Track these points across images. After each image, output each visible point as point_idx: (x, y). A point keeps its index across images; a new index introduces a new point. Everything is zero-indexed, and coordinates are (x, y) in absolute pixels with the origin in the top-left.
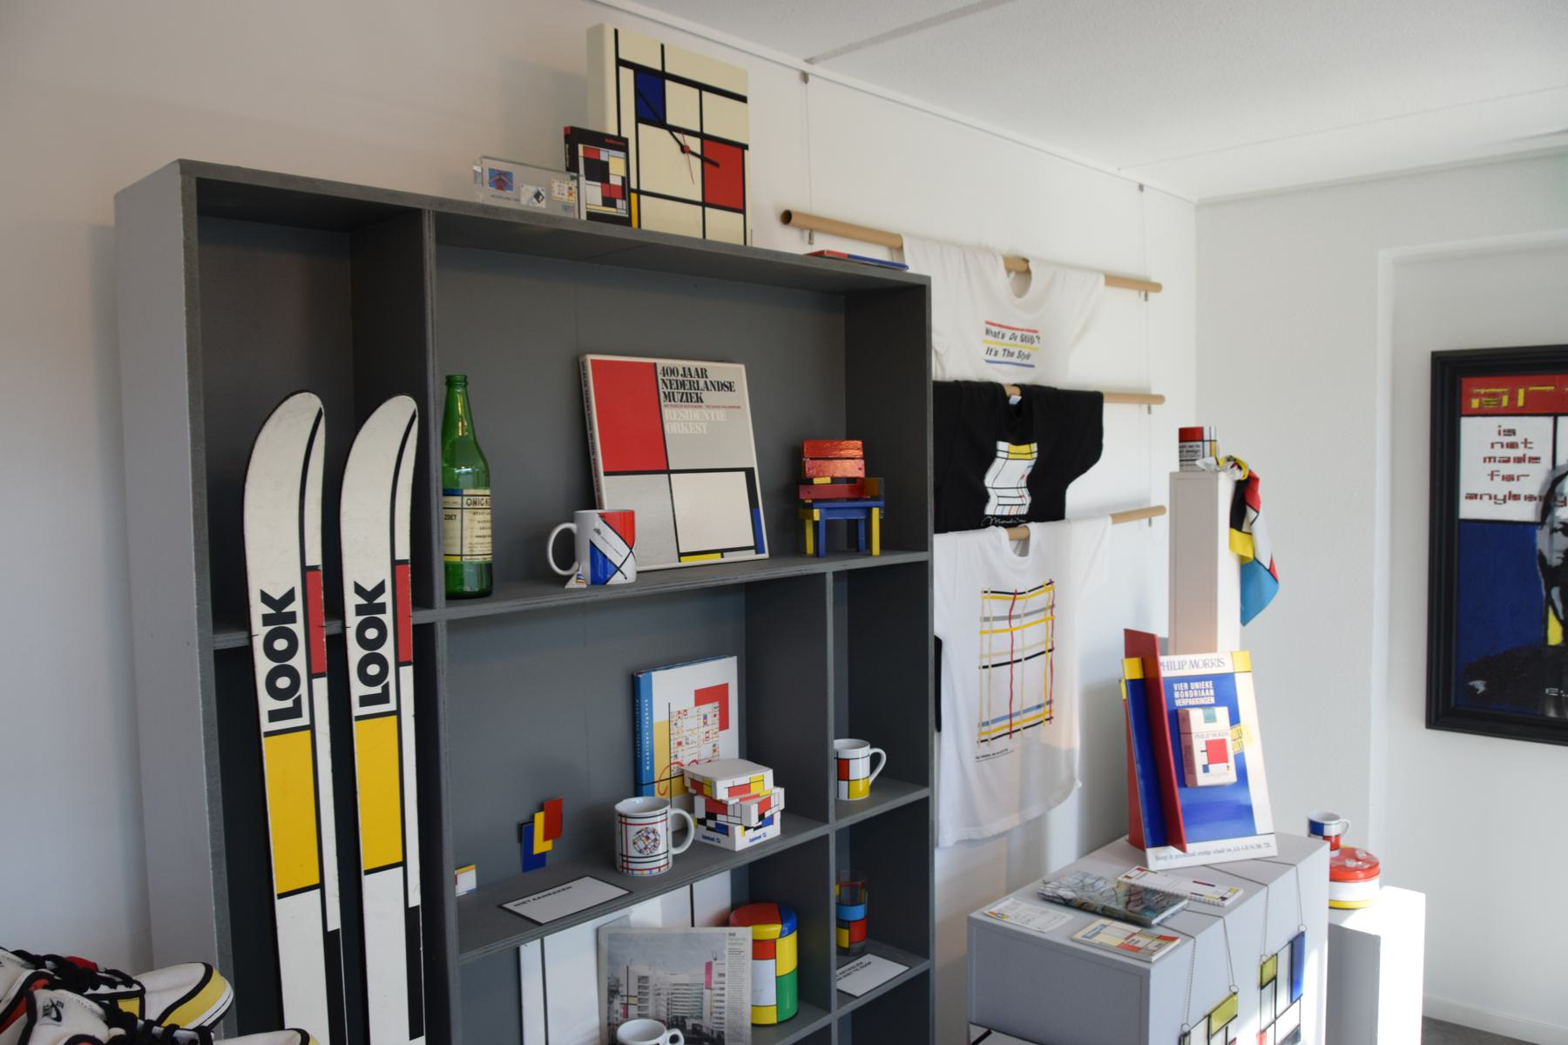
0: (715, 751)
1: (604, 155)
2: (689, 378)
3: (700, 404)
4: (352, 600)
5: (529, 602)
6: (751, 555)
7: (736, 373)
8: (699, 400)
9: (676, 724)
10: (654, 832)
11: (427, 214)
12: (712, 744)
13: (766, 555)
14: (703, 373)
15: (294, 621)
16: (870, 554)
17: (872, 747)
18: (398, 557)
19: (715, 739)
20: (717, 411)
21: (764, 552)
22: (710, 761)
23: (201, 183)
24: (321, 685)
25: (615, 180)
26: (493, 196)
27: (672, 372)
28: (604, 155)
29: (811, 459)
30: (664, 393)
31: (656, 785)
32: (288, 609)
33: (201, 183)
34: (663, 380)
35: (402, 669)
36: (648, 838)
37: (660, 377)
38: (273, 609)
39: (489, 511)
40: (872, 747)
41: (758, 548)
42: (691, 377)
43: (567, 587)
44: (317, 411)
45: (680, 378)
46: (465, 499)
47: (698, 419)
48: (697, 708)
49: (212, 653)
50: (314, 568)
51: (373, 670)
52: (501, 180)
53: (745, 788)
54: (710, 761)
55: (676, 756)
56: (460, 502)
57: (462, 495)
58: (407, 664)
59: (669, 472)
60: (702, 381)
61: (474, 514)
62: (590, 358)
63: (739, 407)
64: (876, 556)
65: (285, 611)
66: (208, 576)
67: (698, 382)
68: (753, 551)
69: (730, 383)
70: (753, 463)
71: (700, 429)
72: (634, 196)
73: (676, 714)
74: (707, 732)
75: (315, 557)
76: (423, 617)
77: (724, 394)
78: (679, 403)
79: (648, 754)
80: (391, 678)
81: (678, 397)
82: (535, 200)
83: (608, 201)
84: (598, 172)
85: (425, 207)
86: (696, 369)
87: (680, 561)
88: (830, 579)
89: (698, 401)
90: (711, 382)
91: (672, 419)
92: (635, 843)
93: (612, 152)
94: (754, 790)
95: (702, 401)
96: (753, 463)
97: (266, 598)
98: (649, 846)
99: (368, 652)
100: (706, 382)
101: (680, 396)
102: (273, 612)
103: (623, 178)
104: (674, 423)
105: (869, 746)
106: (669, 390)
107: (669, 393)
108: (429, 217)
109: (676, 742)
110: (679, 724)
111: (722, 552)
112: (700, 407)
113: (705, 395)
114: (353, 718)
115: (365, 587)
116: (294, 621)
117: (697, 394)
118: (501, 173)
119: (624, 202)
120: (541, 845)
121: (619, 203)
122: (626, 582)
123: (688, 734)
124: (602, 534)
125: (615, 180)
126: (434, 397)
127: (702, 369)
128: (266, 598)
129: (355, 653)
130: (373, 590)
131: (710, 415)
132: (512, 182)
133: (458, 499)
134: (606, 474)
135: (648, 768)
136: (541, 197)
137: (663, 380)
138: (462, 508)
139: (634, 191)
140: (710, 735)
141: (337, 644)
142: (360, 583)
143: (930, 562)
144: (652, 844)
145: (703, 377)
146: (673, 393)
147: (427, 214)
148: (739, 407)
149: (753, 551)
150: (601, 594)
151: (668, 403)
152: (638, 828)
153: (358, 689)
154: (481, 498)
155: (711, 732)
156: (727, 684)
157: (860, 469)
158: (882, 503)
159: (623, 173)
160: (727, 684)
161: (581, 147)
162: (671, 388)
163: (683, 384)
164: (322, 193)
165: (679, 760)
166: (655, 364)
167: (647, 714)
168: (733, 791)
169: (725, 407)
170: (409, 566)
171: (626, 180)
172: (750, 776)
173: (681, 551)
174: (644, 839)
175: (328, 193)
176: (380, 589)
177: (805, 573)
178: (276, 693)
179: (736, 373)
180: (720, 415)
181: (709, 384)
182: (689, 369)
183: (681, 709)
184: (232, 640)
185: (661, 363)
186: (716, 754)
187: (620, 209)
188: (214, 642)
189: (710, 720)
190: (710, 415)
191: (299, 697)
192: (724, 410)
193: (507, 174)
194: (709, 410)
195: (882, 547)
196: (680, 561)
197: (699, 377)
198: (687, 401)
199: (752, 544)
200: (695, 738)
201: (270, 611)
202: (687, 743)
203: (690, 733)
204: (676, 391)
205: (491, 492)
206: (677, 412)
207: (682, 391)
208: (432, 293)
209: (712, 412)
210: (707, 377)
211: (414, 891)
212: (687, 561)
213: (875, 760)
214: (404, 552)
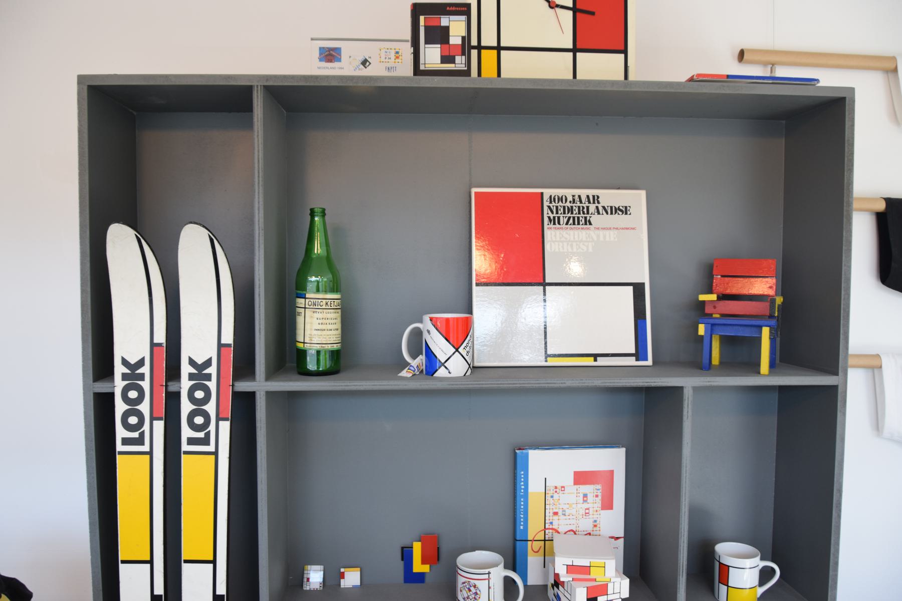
0: (595, 526)
1: (444, 21)
2: (578, 204)
3: (588, 226)
4: (186, 369)
5: (338, 384)
6: (631, 361)
7: (637, 200)
8: (588, 222)
9: (552, 497)
10: (475, 586)
11: (256, 88)
12: (592, 520)
13: (649, 362)
14: (596, 199)
15: (210, 380)
16: (758, 372)
17: (762, 559)
18: (224, 341)
19: (597, 516)
20: (607, 232)
21: (646, 359)
22: (590, 534)
23: (91, 88)
24: (159, 426)
25: (455, 40)
26: (319, 68)
27: (560, 199)
28: (444, 21)
29: (722, 276)
30: (549, 218)
31: (530, 543)
32: (206, 371)
33: (91, 88)
34: (549, 207)
35: (221, 423)
36: (470, 590)
37: (546, 204)
38: (196, 370)
39: (339, 311)
40: (762, 559)
41: (640, 354)
42: (581, 202)
43: (400, 374)
44: (207, 235)
45: (568, 204)
46: (307, 300)
47: (584, 239)
48: (576, 487)
49: (92, 395)
50: (160, 345)
51: (199, 420)
52: (330, 55)
53: (586, 570)
54: (590, 534)
55: (551, 523)
56: (304, 303)
57: (305, 298)
58: (159, 419)
59: (544, 284)
60: (592, 208)
61: (314, 312)
62: (474, 190)
63: (633, 229)
64: (765, 375)
65: (137, 372)
66: (90, 345)
67: (588, 207)
68: (634, 358)
69: (626, 207)
70: (643, 276)
71: (585, 248)
72: (474, 53)
73: (552, 488)
74: (588, 509)
75: (160, 337)
76: (244, 386)
77: (619, 219)
78: (564, 226)
79: (522, 516)
80: (212, 428)
81: (563, 220)
82: (362, 66)
83: (447, 58)
84: (439, 35)
85: (254, 83)
86: (588, 197)
87: (546, 361)
88: (688, 394)
89: (586, 224)
90: (604, 207)
91: (554, 239)
92: (461, 591)
93: (452, 17)
94: (594, 573)
95: (590, 224)
96: (643, 276)
97: (192, 362)
98: (471, 597)
99: (195, 407)
100: (597, 207)
101: (566, 220)
102: (196, 372)
103: (463, 38)
104: (557, 243)
105: (759, 557)
106: (555, 215)
107: (554, 217)
108: (257, 90)
109: (552, 512)
110: (556, 496)
111: (595, 356)
112: (588, 229)
113: (595, 219)
114: (182, 452)
115: (130, 362)
116: (210, 380)
117: (586, 218)
118: (330, 49)
119: (464, 57)
120: (418, 567)
121: (458, 59)
122: (449, 375)
123: (565, 507)
124: (431, 335)
125: (455, 40)
126: (259, 225)
127: (594, 197)
128: (192, 362)
129: (186, 407)
130: (135, 363)
131: (598, 236)
132: (340, 56)
133: (302, 300)
134: (477, 285)
135: (522, 527)
136: (368, 63)
137: (549, 207)
138: (305, 308)
139: (474, 48)
140: (591, 512)
141: (173, 399)
142: (125, 357)
143: (840, 390)
144: (473, 596)
145: (594, 203)
146: (559, 218)
147: (256, 88)
148: (633, 229)
149: (634, 358)
150: (426, 384)
151: (552, 226)
152: (464, 580)
153: (186, 432)
154: (320, 301)
155: (591, 510)
156: (612, 472)
157: (771, 287)
158: (773, 322)
159: (464, 33)
160: (612, 472)
161: (422, 18)
162: (557, 213)
163: (571, 210)
164: (173, 84)
165: (555, 527)
166: (542, 194)
167: (522, 483)
168: (571, 569)
169: (617, 229)
170: (232, 348)
171: (466, 39)
172: (591, 560)
173: (549, 353)
174: (467, 589)
175: (178, 83)
176: (208, 363)
177: (653, 385)
178: (128, 427)
179: (637, 200)
180: (611, 235)
181: (601, 209)
182: (579, 197)
183: (559, 485)
184: (102, 387)
185: (548, 192)
186: (597, 528)
187: (460, 62)
188: (93, 387)
189: (591, 498)
190: (598, 236)
191: (144, 431)
192: (616, 232)
193: (338, 50)
194: (597, 232)
195: (772, 365)
196: (546, 361)
197: (589, 202)
198: (574, 224)
199: (633, 352)
200: (573, 512)
201: (194, 371)
202: (564, 515)
203: (567, 506)
204: (561, 216)
205: (342, 296)
206: (560, 234)
207: (569, 215)
208: (258, 147)
209: (601, 233)
210: (598, 202)
211: (221, 583)
212: (552, 362)
213: (765, 575)
214: (228, 337)
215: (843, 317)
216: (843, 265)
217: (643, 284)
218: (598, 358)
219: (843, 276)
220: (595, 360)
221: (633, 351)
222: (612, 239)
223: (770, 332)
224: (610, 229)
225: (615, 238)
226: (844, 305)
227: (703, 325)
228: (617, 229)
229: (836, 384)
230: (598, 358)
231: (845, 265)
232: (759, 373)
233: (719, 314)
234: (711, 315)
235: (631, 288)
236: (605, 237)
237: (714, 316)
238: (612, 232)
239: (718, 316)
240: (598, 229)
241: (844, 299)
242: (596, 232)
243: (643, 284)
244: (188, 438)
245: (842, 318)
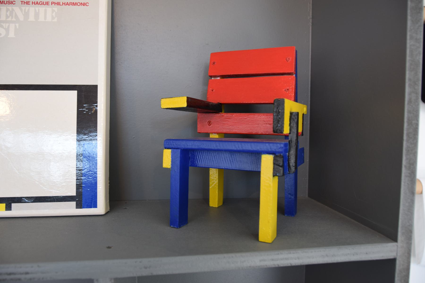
63: (84, 4)
68: (74, 203)
148: (84, 4)
149: (74, 203)
169: (58, 4)
192: (56, 8)
194: (26, 8)
215: (408, 135)
216: (408, 37)
217: (96, 87)
218: (13, 205)
219: (408, 58)
220: (8, 208)
221: (73, 192)
222: (49, 19)
223: (275, 163)
224: (47, 3)
225: (53, 18)
226: (409, 112)
227: (170, 150)
228: (58, 4)
229: (392, 257)
230: (13, 205)
231: (411, 38)
232: (256, 236)
233: (217, 133)
234: (208, 135)
235: (74, 94)
236: (37, 15)
237: (212, 136)
238: (49, 9)
239: (216, 136)
240: (28, 3)
241: (410, 101)
242: (23, 8)
243: (96, 87)
244: (6, 210)
245: (405, 138)
